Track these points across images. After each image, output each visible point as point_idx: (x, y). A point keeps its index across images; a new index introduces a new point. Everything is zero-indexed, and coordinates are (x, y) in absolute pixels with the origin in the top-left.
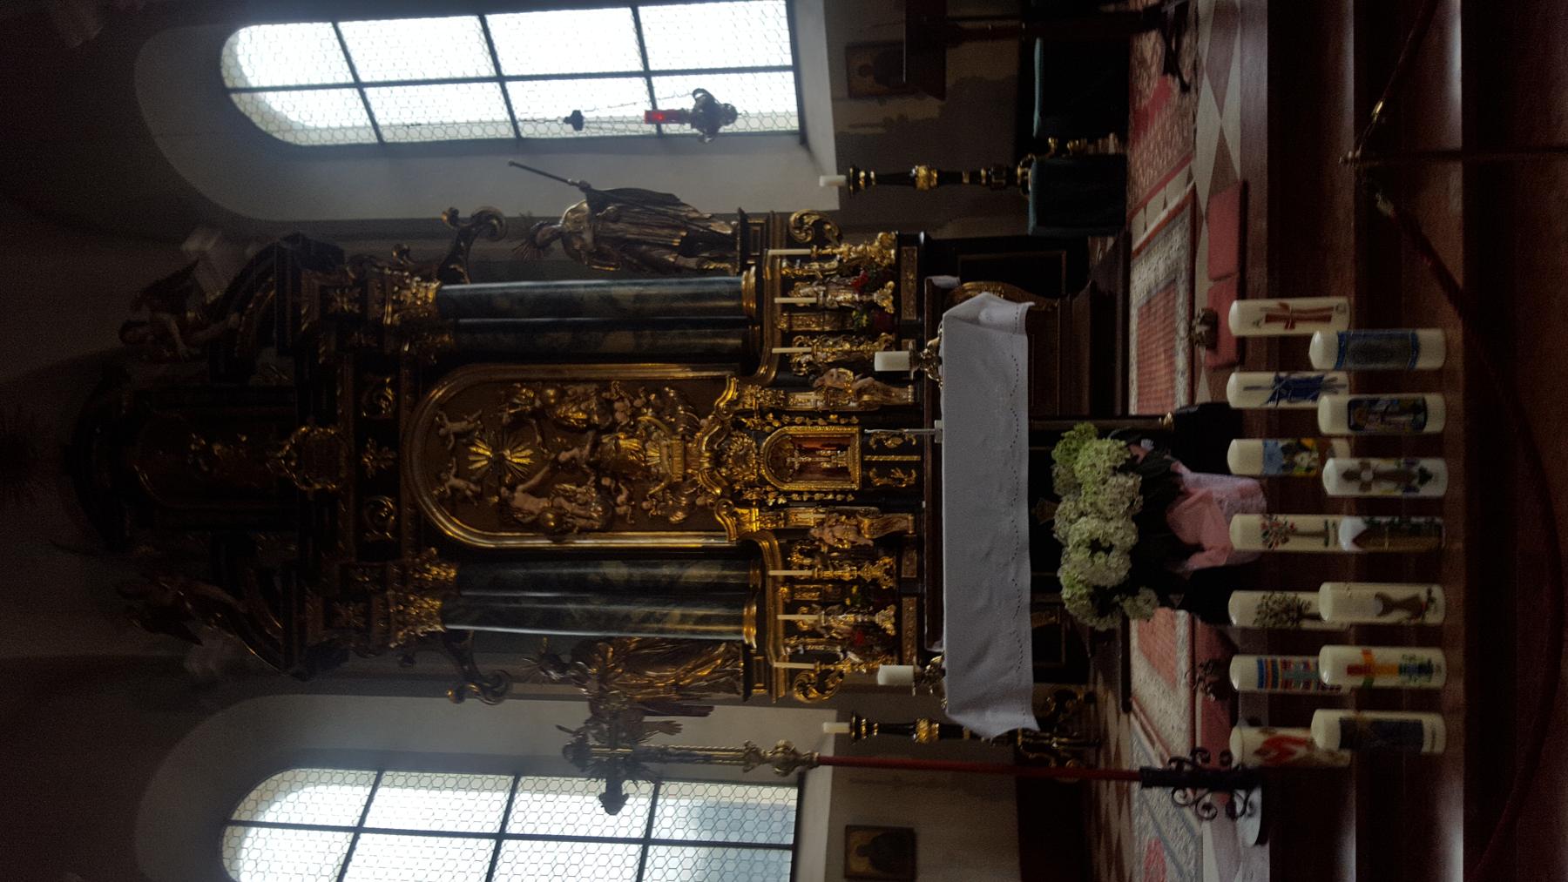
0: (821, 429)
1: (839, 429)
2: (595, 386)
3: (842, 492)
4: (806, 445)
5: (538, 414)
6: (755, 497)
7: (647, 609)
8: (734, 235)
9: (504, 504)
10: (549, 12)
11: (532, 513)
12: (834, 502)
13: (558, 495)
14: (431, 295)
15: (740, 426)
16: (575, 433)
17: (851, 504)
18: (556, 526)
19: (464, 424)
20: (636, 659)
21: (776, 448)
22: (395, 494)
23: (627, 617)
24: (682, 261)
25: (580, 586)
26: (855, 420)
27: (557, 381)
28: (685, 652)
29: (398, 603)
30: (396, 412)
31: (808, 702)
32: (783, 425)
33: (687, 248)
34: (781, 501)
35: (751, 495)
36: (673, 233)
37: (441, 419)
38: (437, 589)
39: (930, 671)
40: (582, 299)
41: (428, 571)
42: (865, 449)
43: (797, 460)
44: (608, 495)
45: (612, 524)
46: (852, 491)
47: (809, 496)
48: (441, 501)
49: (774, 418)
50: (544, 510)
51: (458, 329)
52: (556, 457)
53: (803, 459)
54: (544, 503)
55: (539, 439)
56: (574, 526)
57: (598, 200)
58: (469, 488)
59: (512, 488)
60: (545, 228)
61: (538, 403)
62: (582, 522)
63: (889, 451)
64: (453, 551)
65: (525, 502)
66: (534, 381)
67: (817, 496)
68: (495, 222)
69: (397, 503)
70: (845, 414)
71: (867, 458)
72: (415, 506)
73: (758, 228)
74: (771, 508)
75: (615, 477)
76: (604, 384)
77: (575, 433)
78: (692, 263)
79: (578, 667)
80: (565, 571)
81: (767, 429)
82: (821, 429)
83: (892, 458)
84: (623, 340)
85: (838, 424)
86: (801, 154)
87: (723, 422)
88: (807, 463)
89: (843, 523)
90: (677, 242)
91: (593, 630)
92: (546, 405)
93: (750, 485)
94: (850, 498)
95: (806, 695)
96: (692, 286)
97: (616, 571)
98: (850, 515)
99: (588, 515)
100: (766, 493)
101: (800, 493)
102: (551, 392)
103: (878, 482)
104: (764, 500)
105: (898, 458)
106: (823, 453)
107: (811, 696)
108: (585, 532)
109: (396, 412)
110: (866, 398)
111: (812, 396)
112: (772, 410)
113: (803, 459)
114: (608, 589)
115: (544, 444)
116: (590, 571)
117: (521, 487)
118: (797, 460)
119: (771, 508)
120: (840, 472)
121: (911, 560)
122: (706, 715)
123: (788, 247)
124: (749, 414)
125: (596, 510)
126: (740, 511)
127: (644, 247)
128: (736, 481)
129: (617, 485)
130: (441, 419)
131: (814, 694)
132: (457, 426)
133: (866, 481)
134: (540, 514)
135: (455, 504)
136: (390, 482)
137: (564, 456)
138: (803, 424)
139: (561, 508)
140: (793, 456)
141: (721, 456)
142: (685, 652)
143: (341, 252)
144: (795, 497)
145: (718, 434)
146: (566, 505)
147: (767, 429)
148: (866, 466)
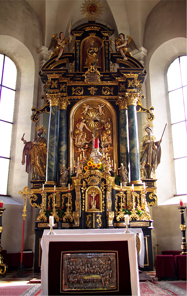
2: (111, 143)
4: (97, 198)
5: (104, 128)
11: (79, 127)
13: (83, 133)
17: (82, 210)
18: (75, 133)
19: (101, 111)
24: (144, 165)
25: (60, 140)
29: (57, 96)
30: (104, 95)
34: (82, 191)
42: (96, 213)
45: (76, 147)
46: (85, 210)
48: (82, 105)
50: (79, 130)
52: (93, 133)
54: (82, 130)
56: (75, 138)
61: (107, 129)
64: (69, 108)
65: (82, 125)
68: (151, 119)
69: (81, 95)
71: (94, 214)
72: (81, 99)
73: (153, 185)
74: (81, 189)
75: (88, 148)
76: (112, 145)
80: (64, 136)
81: (101, 188)
83: (94, 221)
85: (103, 206)
86: (172, 195)
90: (148, 164)
92: (106, 131)
93: (86, 183)
94: (83, 209)
97: (64, 148)
99: (78, 141)
100: (85, 187)
101: (85, 196)
102: (110, 132)
103: (88, 217)
106: (95, 202)
108: (74, 140)
109: (104, 95)
112: (106, 189)
114: (59, 146)
116: (63, 143)
117: (85, 124)
119: (81, 189)
121: (67, 226)
122: (26, 171)
124: (105, 183)
127: (147, 155)
133: (87, 214)
135: (81, 108)
136: (87, 93)
137: (93, 135)
138: (103, 197)
144: (84, 195)
146: (81, 135)
148: (92, 214)
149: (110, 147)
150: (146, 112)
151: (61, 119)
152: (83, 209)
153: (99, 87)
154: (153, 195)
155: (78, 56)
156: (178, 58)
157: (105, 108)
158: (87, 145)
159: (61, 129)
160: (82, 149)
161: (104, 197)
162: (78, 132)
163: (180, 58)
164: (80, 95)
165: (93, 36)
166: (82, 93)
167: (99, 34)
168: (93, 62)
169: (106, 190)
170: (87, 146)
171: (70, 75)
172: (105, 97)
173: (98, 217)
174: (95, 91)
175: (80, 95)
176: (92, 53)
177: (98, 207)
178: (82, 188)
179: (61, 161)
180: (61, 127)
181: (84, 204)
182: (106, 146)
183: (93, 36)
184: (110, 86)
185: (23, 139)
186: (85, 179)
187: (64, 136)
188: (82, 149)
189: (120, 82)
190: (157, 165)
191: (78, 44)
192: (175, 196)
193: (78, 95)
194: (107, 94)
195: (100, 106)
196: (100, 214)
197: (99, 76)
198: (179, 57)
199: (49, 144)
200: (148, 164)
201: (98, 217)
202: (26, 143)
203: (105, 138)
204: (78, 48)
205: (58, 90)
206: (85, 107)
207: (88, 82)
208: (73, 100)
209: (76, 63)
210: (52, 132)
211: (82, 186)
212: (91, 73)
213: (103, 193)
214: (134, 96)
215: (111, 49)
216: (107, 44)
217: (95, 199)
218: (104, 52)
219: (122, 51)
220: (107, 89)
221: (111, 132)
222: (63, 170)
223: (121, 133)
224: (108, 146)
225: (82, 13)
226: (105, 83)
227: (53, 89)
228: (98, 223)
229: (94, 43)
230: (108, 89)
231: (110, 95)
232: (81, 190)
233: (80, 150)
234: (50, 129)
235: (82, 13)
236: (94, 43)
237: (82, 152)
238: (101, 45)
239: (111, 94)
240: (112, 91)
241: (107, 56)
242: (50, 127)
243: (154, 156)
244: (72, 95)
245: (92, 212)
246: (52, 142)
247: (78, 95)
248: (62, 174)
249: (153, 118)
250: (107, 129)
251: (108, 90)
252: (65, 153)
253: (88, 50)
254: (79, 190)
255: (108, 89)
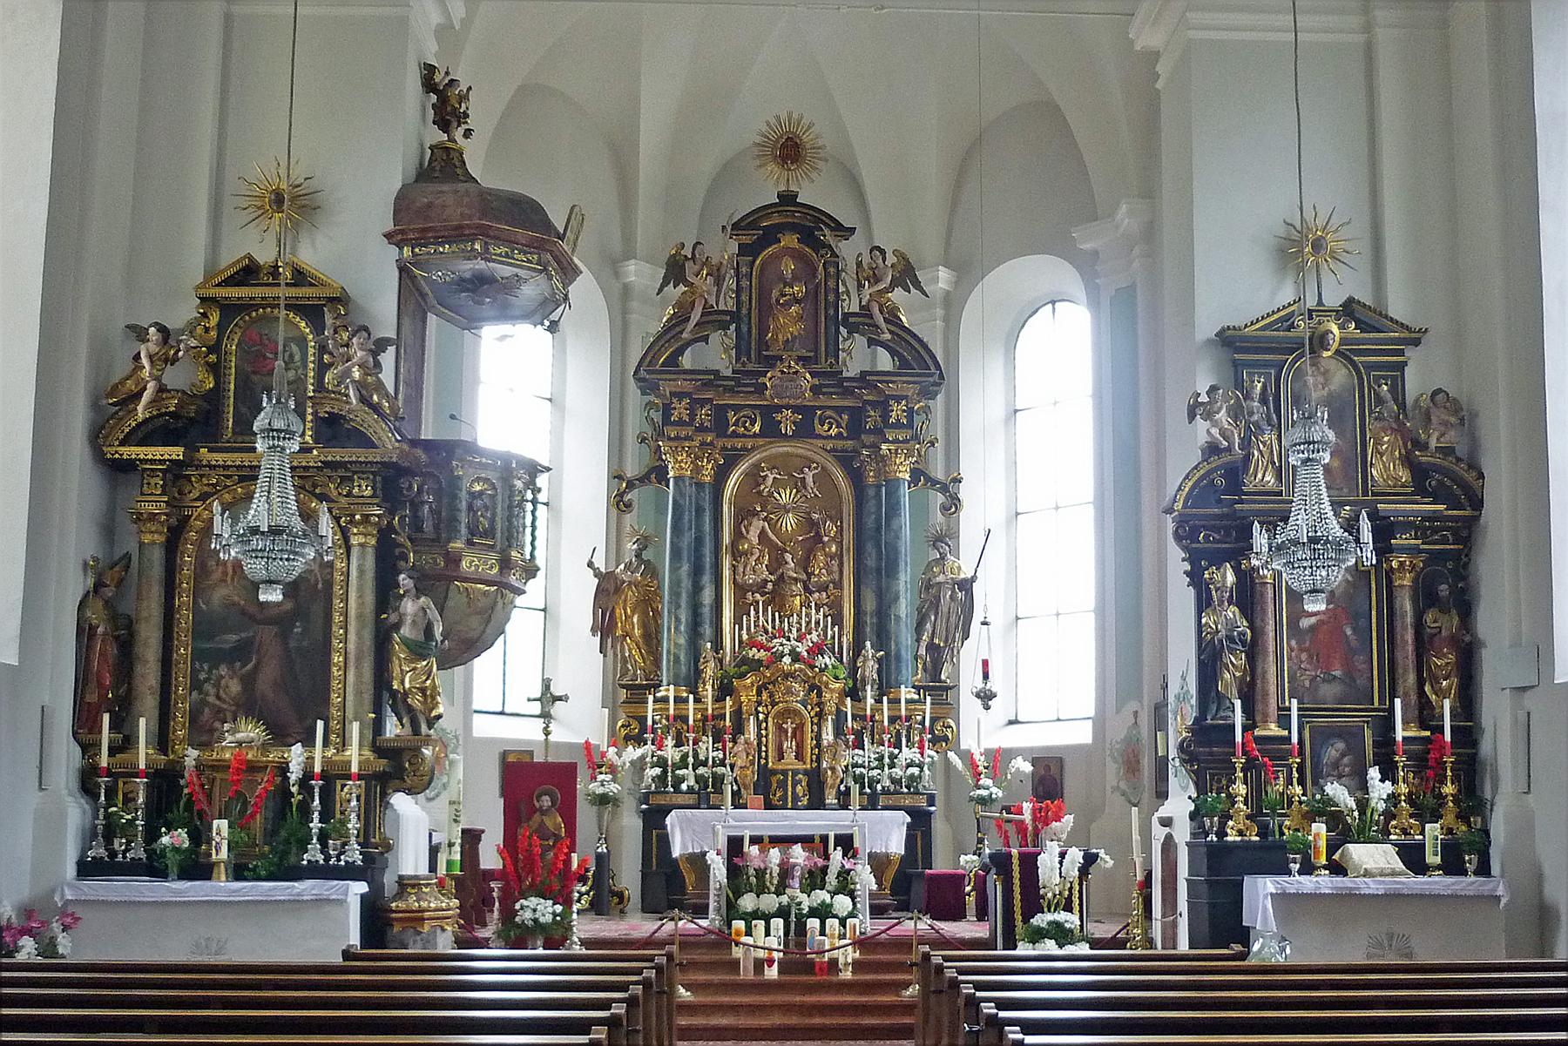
0: (809, 743)
1: (809, 755)
2: (837, 578)
3: (767, 755)
5: (818, 538)
6: (764, 698)
7: (683, 620)
8: (940, 681)
9: (755, 514)
10: (1094, 642)
11: (748, 533)
12: (760, 751)
13: (760, 551)
14: (901, 475)
15: (812, 688)
16: (805, 564)
18: (738, 550)
20: (648, 603)
21: (797, 713)
22: (762, 434)
23: (678, 607)
24: (923, 645)
25: (697, 572)
26: (815, 765)
27: (842, 552)
28: (651, 639)
30: (820, 437)
31: (618, 728)
32: (811, 718)
33: (931, 647)
34: (761, 716)
35: (765, 696)
36: (943, 638)
37: (816, 468)
38: (697, 470)
39: (436, 506)
40: (897, 579)
41: (709, 462)
42: (795, 773)
43: (789, 726)
44: (760, 587)
45: (740, 590)
46: (767, 763)
47: (764, 734)
48: (757, 467)
49: (816, 712)
51: (879, 487)
53: (790, 730)
54: (755, 540)
55: (801, 538)
57: (966, 586)
58: (765, 488)
59: (765, 519)
60: (947, 548)
61: (826, 539)
62: (741, 569)
63: (794, 788)
64: (722, 475)
65: (757, 525)
66: (842, 536)
67: (764, 739)
68: (953, 509)
69: (755, 435)
70: (819, 760)
72: (753, 448)
73: (944, 697)
74: (756, 709)
76: (839, 585)
77: (805, 564)
78: (922, 651)
79: (638, 566)
81: (809, 707)
82: (809, 743)
83: (790, 789)
84: (870, 605)
85: (812, 754)
87: (814, 678)
88: (787, 733)
89: (747, 757)
90: (936, 641)
91: (670, 582)
93: (771, 695)
95: (623, 726)
96: (907, 655)
97: (707, 596)
98: (752, 763)
99: (746, 573)
102: (834, 549)
103: (774, 779)
104: (761, 704)
105: (790, 793)
106: (794, 743)
107: (622, 730)
108: (734, 568)
109: (820, 437)
110: (829, 772)
111: (831, 738)
112: (821, 710)
113: (790, 730)
114: (697, 589)
115: (797, 542)
116: (707, 579)
118: (789, 726)
120: (781, 756)
123: (931, 718)
124: (819, 695)
125: (750, 579)
126: (755, 688)
127: (933, 618)
128: (774, 686)
129: (767, 593)
130: (816, 468)
131: (624, 732)
132: (809, 480)
133: (774, 772)
134: (746, 538)
135: (754, 477)
136: (771, 431)
137: (788, 557)
138: (812, 731)
139: (752, 554)
140: (792, 723)
141: (792, 677)
142: (651, 639)
143: (933, 397)
144: (764, 724)
145: (806, 674)
146: (754, 558)
147: (809, 707)
148: (784, 773)
149: (834, 589)
150: (940, 488)
151: (699, 511)
152: (763, 761)
153: (807, 411)
154: (943, 726)
155: (744, 311)
156: (1050, 305)
157: (824, 477)
158: (770, 586)
159: (699, 541)
160: (757, 595)
161: (816, 729)
162: (746, 546)
163: (1057, 304)
164: (750, 436)
165: (790, 240)
166: (757, 428)
167: (809, 236)
168: (792, 334)
169: (821, 715)
170: (771, 587)
171: (722, 383)
172: (829, 404)
173: (800, 781)
174: (794, 423)
175: (750, 436)
176: (788, 305)
177: (799, 756)
178: (760, 709)
179: (701, 630)
180: (699, 534)
181: (764, 748)
182: (823, 588)
183: (790, 240)
184: (839, 410)
185: (590, 564)
186: (769, 684)
187: (708, 560)
188: (756, 594)
189: (868, 402)
190: (960, 642)
191: (744, 270)
192: (1011, 723)
193: (744, 436)
194: (829, 433)
195: (807, 470)
196: (806, 772)
197: (808, 382)
198: (1053, 302)
199: (670, 588)
200: (936, 641)
201: (800, 781)
202: (597, 574)
203: (821, 564)
204: (745, 283)
205: (689, 431)
206: (765, 474)
207: (776, 401)
208: (730, 450)
209: (738, 330)
210: (676, 553)
211: (759, 704)
212: (783, 372)
213: (812, 722)
214: (905, 451)
215: (844, 284)
216: (832, 270)
217: (794, 735)
218: (823, 297)
219: (876, 310)
220: (830, 417)
221: (837, 548)
222: (705, 657)
223: (866, 555)
224: (828, 586)
225: (758, 162)
226: (823, 400)
227: (675, 423)
228: (800, 795)
229: (792, 270)
230: (834, 419)
231: (839, 436)
232: (758, 712)
233: (751, 598)
234: (672, 542)
235: (758, 162)
236: (792, 270)
237: (757, 602)
238: (815, 277)
239: (841, 433)
240: (844, 425)
241: (831, 312)
242: (672, 539)
243: (953, 619)
244: (729, 433)
245: (785, 767)
246: (676, 584)
247: (744, 436)
248: (702, 667)
249: (956, 508)
250: (826, 539)
251: (832, 420)
252: (712, 609)
253: (775, 294)
254: (754, 712)
255: (834, 419)
